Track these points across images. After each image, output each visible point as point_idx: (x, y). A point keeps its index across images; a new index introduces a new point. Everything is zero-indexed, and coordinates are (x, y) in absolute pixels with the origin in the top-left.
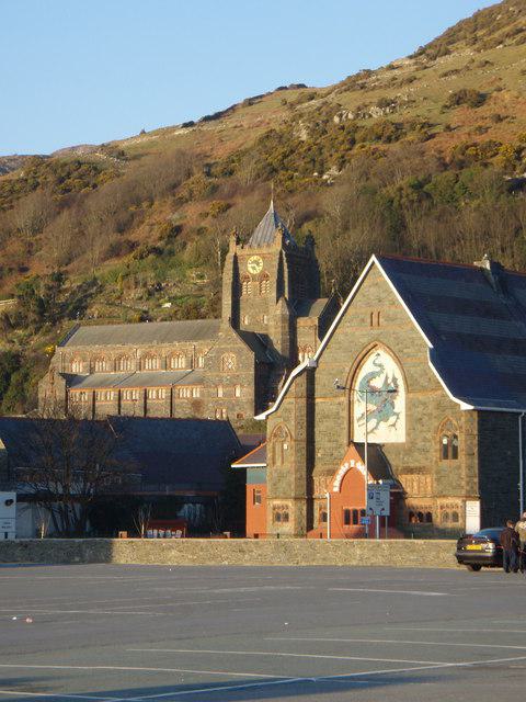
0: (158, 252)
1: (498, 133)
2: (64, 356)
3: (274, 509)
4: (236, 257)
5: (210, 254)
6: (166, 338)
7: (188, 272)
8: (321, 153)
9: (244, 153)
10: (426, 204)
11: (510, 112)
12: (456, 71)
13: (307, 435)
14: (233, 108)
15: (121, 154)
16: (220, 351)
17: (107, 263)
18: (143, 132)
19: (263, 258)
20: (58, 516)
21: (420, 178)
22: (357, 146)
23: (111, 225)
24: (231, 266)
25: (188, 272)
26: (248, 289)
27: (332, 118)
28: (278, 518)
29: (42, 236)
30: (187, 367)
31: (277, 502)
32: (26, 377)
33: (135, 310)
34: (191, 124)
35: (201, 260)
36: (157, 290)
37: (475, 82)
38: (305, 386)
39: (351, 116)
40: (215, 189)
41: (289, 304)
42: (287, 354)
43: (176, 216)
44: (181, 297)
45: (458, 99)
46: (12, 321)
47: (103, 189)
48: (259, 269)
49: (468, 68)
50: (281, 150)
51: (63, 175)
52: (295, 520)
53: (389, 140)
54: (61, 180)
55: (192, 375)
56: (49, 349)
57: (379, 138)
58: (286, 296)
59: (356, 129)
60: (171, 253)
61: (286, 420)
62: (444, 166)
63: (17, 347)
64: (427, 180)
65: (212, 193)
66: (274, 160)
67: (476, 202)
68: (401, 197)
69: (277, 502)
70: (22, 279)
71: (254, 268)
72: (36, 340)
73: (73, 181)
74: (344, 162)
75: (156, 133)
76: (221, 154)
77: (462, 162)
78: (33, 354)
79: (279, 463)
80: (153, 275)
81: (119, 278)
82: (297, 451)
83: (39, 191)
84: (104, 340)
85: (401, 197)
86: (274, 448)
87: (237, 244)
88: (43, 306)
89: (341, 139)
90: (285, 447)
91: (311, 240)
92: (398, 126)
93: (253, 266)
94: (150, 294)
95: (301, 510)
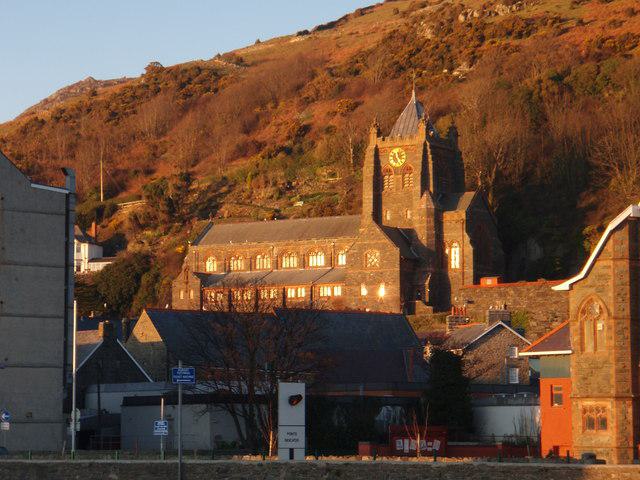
0: (288, 151)
2: (197, 254)
3: (585, 411)
4: (377, 150)
5: (342, 152)
6: (303, 235)
7: (319, 171)
8: (449, 51)
9: (371, 52)
10: (566, 96)
13: (632, 311)
14: (346, 18)
15: (240, 61)
16: (363, 248)
17: (234, 163)
18: (258, 42)
20: (242, 421)
21: (559, 70)
22: (487, 42)
23: (237, 126)
24: (372, 159)
25: (319, 171)
26: (390, 183)
28: (590, 424)
29: (167, 139)
30: (299, 266)
31: (589, 403)
32: (157, 277)
33: (267, 210)
34: (306, 32)
35: (333, 158)
36: (288, 189)
38: (626, 245)
39: (476, 15)
40: (342, 88)
41: (434, 197)
42: (433, 248)
43: (303, 115)
44: (313, 196)
46: (141, 221)
47: (228, 91)
48: (400, 163)
50: (407, 48)
51: (184, 80)
52: (617, 427)
53: (520, 35)
54: (182, 86)
55: (331, 273)
56: (180, 249)
57: (509, 33)
58: (431, 189)
59: (484, 26)
60: (301, 151)
61: (601, 290)
62: (582, 61)
63: (147, 247)
64: (567, 72)
66: (401, 57)
67: (621, 93)
69: (589, 403)
70: (150, 181)
71: (395, 160)
72: (165, 241)
73: (195, 86)
74: (474, 58)
75: (271, 42)
76: (340, 58)
77: (601, 55)
78: (163, 255)
79: (589, 348)
80: (283, 174)
81: (249, 177)
82: (618, 333)
83: (160, 96)
84: (238, 238)
86: (582, 329)
87: (378, 136)
88: (172, 206)
89: (469, 35)
90: (600, 326)
91: (453, 130)
92: (529, 22)
93: (397, 156)
94: (281, 193)
95: (624, 413)
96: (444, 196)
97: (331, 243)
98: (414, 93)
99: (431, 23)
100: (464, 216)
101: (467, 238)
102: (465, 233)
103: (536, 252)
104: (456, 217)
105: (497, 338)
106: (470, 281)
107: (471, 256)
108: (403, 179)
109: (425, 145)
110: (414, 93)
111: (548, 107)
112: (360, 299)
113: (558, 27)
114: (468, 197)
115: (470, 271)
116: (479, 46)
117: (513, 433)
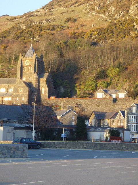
1: (83, 29)
4: (21, 60)
5: (5, 60)
10: (68, 48)
11: (84, 24)
12: (65, 12)
16: (18, 87)
19: (30, 61)
24: (20, 63)
26: (25, 69)
27: (32, 24)
37: (73, 15)
39: (38, 23)
45: (69, 20)
48: (28, 64)
49: (13, 27)
53: (52, 30)
57: (49, 29)
58: (37, 72)
59: (41, 27)
64: (67, 41)
65: (1, 42)
68: (61, 45)
71: (28, 62)
85: (61, 45)
92: (54, 26)
96: (39, 73)
97: (7, 85)
98: (32, 45)
99: (25, 24)
100: (46, 80)
101: (46, 86)
102: (46, 84)
103: (62, 90)
104: (43, 80)
105: (69, 113)
106: (47, 97)
107: (47, 91)
108: (29, 68)
109: (35, 60)
110: (32, 45)
111: (63, 51)
112: (23, 101)
113: (62, 28)
114: (46, 75)
115: (47, 95)
116: (40, 32)
117: (98, 139)
